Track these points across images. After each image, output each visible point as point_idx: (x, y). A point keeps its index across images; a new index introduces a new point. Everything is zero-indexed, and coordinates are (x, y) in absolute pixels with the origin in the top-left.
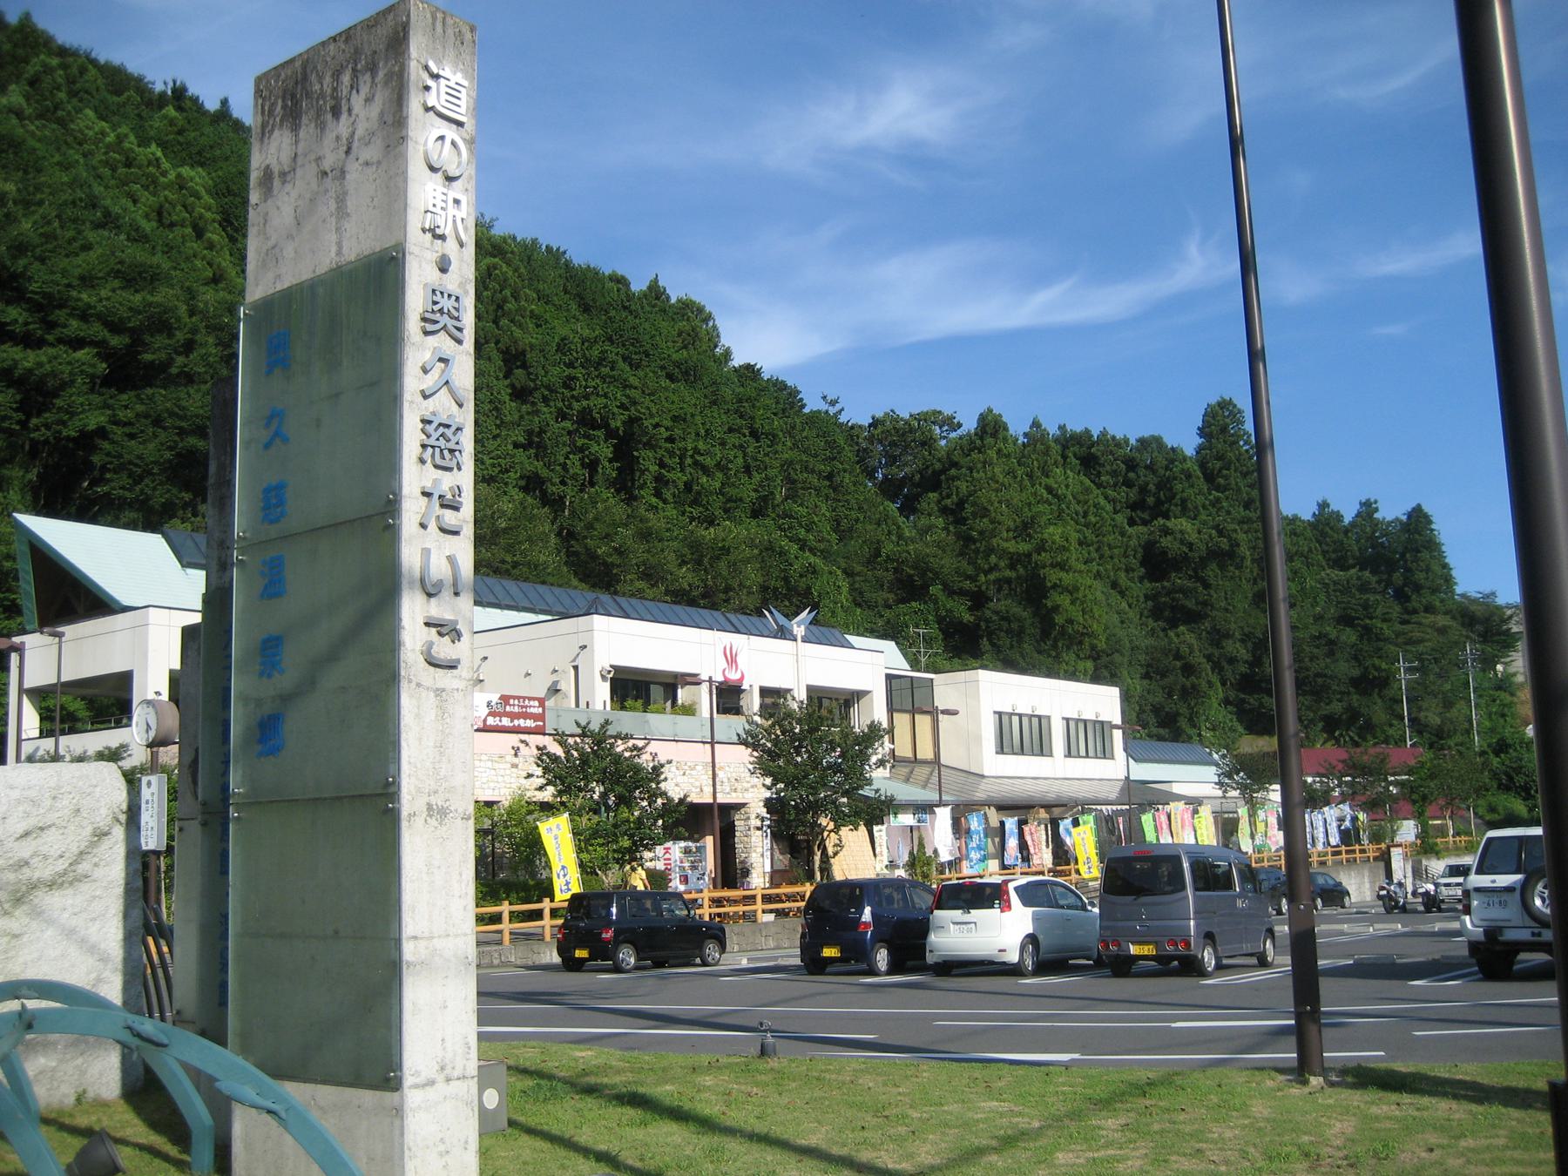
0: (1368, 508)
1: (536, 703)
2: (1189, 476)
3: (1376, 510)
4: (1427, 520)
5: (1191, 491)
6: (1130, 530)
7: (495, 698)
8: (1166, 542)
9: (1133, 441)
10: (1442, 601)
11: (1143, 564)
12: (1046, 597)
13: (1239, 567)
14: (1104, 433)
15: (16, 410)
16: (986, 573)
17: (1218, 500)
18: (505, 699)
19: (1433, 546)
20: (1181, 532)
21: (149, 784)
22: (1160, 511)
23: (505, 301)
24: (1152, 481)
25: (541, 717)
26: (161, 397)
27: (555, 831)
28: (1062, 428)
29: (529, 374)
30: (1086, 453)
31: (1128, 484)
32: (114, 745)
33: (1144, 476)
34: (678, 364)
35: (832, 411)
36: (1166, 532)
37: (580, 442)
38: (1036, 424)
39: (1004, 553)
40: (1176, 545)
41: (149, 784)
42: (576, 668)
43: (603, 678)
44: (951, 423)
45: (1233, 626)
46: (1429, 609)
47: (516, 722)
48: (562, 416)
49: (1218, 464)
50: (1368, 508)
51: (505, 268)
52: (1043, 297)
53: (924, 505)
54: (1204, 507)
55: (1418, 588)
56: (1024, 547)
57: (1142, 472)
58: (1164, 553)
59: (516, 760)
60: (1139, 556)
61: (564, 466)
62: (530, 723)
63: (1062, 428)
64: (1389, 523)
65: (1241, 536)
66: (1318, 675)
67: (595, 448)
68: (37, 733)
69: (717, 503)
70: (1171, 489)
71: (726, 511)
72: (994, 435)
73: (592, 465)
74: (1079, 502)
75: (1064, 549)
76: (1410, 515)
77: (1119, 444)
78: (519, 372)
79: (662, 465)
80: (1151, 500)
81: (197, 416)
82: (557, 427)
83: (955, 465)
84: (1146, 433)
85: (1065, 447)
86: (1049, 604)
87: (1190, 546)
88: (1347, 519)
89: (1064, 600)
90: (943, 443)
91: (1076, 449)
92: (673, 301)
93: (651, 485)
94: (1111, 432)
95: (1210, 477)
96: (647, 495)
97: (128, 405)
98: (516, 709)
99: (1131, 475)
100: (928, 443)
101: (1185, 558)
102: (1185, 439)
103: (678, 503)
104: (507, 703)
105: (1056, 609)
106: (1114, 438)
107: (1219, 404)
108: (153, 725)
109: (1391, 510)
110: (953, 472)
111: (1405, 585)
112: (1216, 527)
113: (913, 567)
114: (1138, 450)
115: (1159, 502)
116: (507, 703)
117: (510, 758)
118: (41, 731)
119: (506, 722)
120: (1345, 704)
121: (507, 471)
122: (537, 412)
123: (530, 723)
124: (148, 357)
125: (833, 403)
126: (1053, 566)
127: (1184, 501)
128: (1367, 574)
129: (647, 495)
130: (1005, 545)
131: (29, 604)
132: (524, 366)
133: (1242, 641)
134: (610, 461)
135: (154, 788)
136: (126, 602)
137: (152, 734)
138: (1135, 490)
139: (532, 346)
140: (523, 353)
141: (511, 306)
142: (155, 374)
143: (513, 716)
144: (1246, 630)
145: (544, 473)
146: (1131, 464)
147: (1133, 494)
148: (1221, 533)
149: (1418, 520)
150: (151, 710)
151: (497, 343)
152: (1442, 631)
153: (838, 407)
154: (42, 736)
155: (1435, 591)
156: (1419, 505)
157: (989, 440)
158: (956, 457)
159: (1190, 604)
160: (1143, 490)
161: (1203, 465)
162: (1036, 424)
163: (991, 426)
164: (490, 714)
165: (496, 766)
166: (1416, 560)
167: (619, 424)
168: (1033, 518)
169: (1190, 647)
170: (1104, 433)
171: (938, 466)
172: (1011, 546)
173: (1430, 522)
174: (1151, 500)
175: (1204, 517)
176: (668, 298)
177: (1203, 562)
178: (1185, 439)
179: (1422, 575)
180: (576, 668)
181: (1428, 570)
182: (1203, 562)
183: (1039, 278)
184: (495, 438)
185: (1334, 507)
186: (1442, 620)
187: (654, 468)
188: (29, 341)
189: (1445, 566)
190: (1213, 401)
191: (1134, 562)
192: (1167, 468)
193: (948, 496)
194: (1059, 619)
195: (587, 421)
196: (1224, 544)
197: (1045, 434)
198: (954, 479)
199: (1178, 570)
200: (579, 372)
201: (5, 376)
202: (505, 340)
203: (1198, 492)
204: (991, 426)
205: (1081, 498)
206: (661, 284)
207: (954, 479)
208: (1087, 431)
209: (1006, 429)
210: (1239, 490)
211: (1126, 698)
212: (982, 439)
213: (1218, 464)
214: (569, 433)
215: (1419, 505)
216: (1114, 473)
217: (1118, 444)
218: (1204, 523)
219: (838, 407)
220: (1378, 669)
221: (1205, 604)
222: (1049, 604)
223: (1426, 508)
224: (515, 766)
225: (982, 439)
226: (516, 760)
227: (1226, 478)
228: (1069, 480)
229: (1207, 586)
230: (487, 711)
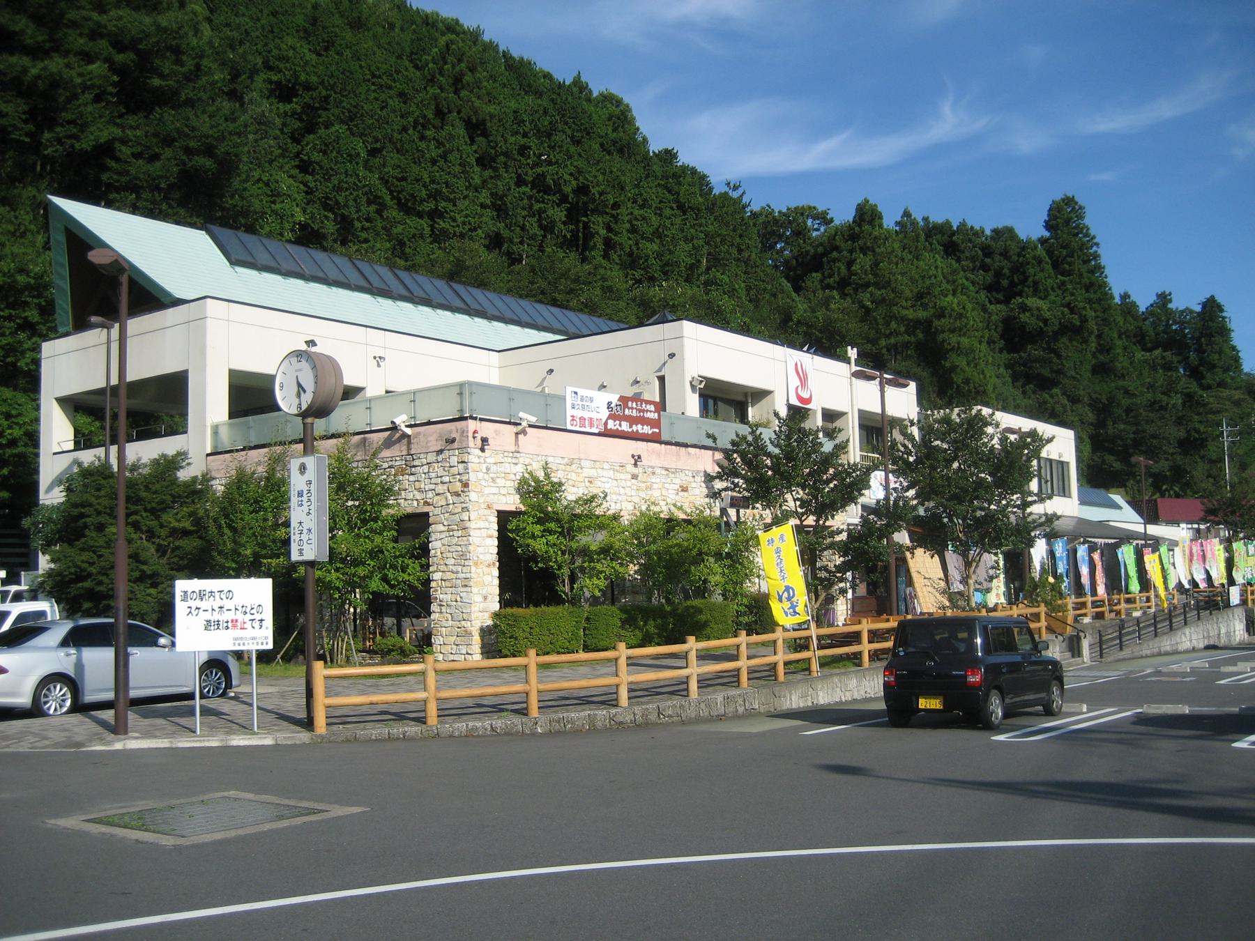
0: (1164, 298)
1: (652, 408)
2: (1040, 262)
3: (1170, 301)
4: (1220, 308)
5: (1041, 275)
6: (992, 307)
7: (614, 399)
8: (1025, 317)
9: (988, 232)
10: (1232, 378)
11: (1002, 336)
12: (946, 359)
13: (1085, 341)
14: (963, 224)
15: (26, 122)
16: (888, 336)
17: (1063, 283)
18: (624, 400)
19: (1224, 332)
20: (1038, 309)
21: (303, 468)
22: (1009, 294)
23: (462, 74)
24: (1006, 265)
25: (655, 423)
26: (170, 119)
27: (777, 543)
28: (926, 219)
29: (489, 142)
30: (949, 240)
31: (985, 268)
32: (171, 452)
33: (997, 262)
34: (614, 142)
35: (735, 195)
36: (1024, 308)
37: (536, 206)
38: (907, 214)
39: (903, 319)
40: (1034, 320)
41: (303, 468)
42: (662, 379)
43: (693, 387)
44: (824, 218)
45: (1082, 392)
46: (1222, 384)
47: (634, 428)
48: (520, 182)
49: (1064, 252)
50: (1164, 298)
51: (461, 44)
52: (823, 147)
53: (809, 283)
54: (1053, 289)
55: (1212, 367)
56: (922, 314)
57: (997, 258)
58: (1023, 327)
59: (635, 471)
60: (999, 329)
61: (523, 228)
62: (647, 430)
63: (926, 219)
64: (1182, 312)
65: (1091, 314)
66: (1154, 436)
67: (550, 212)
68: (71, 446)
69: (655, 266)
70: (1024, 272)
71: (665, 273)
72: (871, 222)
73: (547, 228)
74: (948, 282)
75: (960, 316)
76: (1204, 305)
77: (978, 234)
78: (480, 140)
79: (609, 229)
80: (1005, 283)
81: (207, 137)
82: (517, 192)
83: (836, 248)
84: (1000, 225)
85: (928, 236)
86: (948, 365)
87: (1045, 321)
88: (1142, 309)
89: (961, 362)
90: (815, 234)
91: (939, 236)
92: (595, 94)
93: (600, 246)
94: (969, 224)
95: (1056, 265)
96: (597, 254)
97: (137, 129)
98: (634, 413)
99: (988, 260)
100: (801, 233)
101: (1041, 333)
102: (1031, 228)
103: (623, 266)
104: (626, 406)
105: (954, 368)
106: (972, 228)
107: (1063, 200)
108: (309, 385)
109: (1187, 300)
110: (835, 254)
111: (1199, 365)
112: (1068, 305)
113: (821, 332)
114: (992, 238)
115: (1013, 284)
116: (626, 406)
117: (630, 468)
118: (77, 443)
119: (625, 426)
120: (1171, 463)
121: (475, 229)
122: (498, 177)
123: (647, 430)
124: (156, 82)
125: (736, 188)
126: (952, 331)
127: (1036, 283)
128: (1168, 354)
129: (597, 254)
130: (905, 312)
131: (64, 305)
132: (485, 134)
133: (1090, 405)
134: (564, 223)
135: (311, 474)
136: (178, 293)
137: (307, 399)
138: (991, 273)
139: (492, 116)
140: (484, 122)
141: (468, 78)
142: (167, 98)
143: (632, 421)
144: (1094, 396)
145: (506, 233)
146: (987, 251)
147: (989, 277)
148: (1072, 311)
149: (1212, 308)
150: (305, 365)
151: (459, 113)
152: (1237, 403)
153: (740, 191)
154: (78, 447)
155: (1227, 370)
156: (1213, 297)
157: (866, 227)
158: (838, 241)
159: (1046, 372)
160: (999, 274)
161: (1050, 253)
162: (907, 214)
163: (867, 215)
164: (610, 417)
165: (618, 476)
166: (1211, 343)
167: (569, 190)
168: (928, 288)
169: (1064, 407)
170: (963, 224)
171: (820, 250)
172: (910, 314)
173: (1222, 311)
174: (1005, 283)
175: (1052, 298)
176: (591, 92)
177: (1056, 335)
178: (1031, 228)
179: (1216, 357)
180: (662, 379)
181: (1220, 352)
182: (1056, 335)
183: (821, 131)
184: (465, 198)
185: (1133, 298)
186: (1237, 395)
187: (603, 232)
188: (37, 52)
189: (1234, 348)
190: (1058, 197)
191: (996, 336)
192: (1019, 255)
193: (830, 276)
194: (958, 379)
195: (540, 184)
196: (1076, 320)
197: (914, 223)
198: (834, 261)
199: (1034, 342)
200: (533, 142)
201: (17, 86)
202: (466, 111)
203: (1046, 276)
204: (867, 215)
205: (950, 278)
206: (583, 79)
207: (834, 261)
208: (948, 223)
209: (881, 217)
210: (1081, 275)
211: (1079, 440)
212: (860, 226)
213: (1064, 252)
214: (530, 198)
215: (1213, 297)
216: (973, 259)
217: (976, 234)
218: (1054, 302)
219: (740, 191)
220: (1198, 431)
221: (1059, 372)
222: (948, 365)
223: (1219, 299)
224: (634, 477)
225: (860, 226)
226: (635, 471)
227: (1070, 264)
228: (936, 263)
229: (1059, 357)
230: (607, 413)
